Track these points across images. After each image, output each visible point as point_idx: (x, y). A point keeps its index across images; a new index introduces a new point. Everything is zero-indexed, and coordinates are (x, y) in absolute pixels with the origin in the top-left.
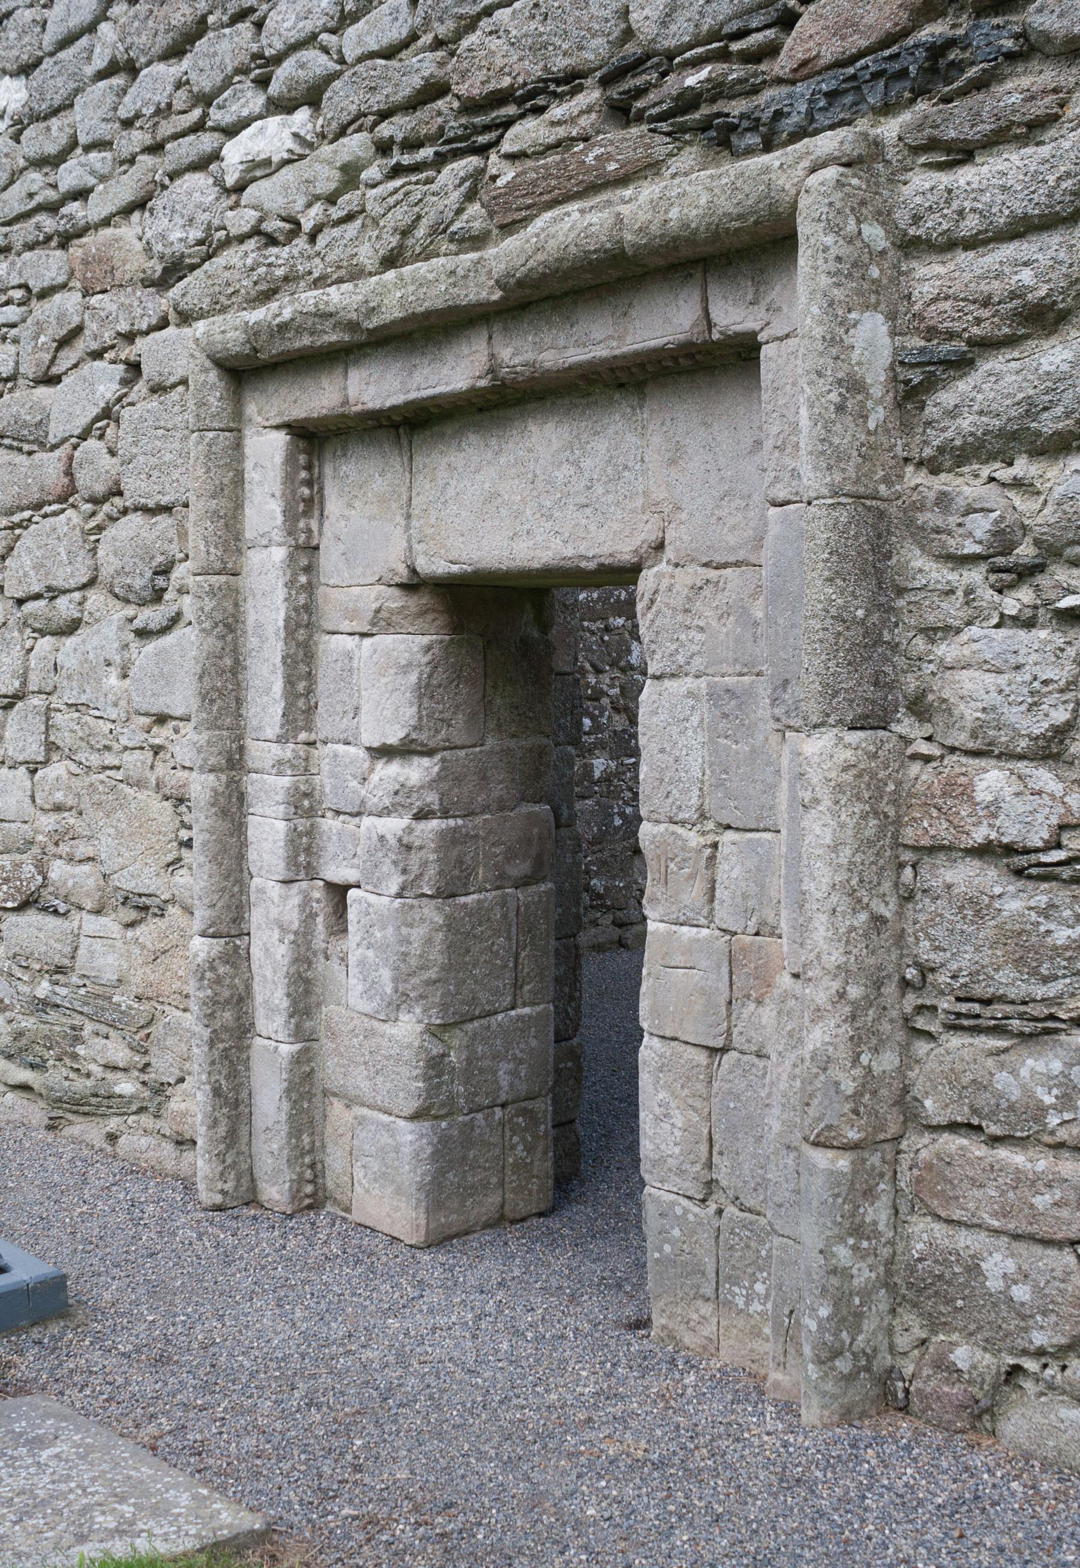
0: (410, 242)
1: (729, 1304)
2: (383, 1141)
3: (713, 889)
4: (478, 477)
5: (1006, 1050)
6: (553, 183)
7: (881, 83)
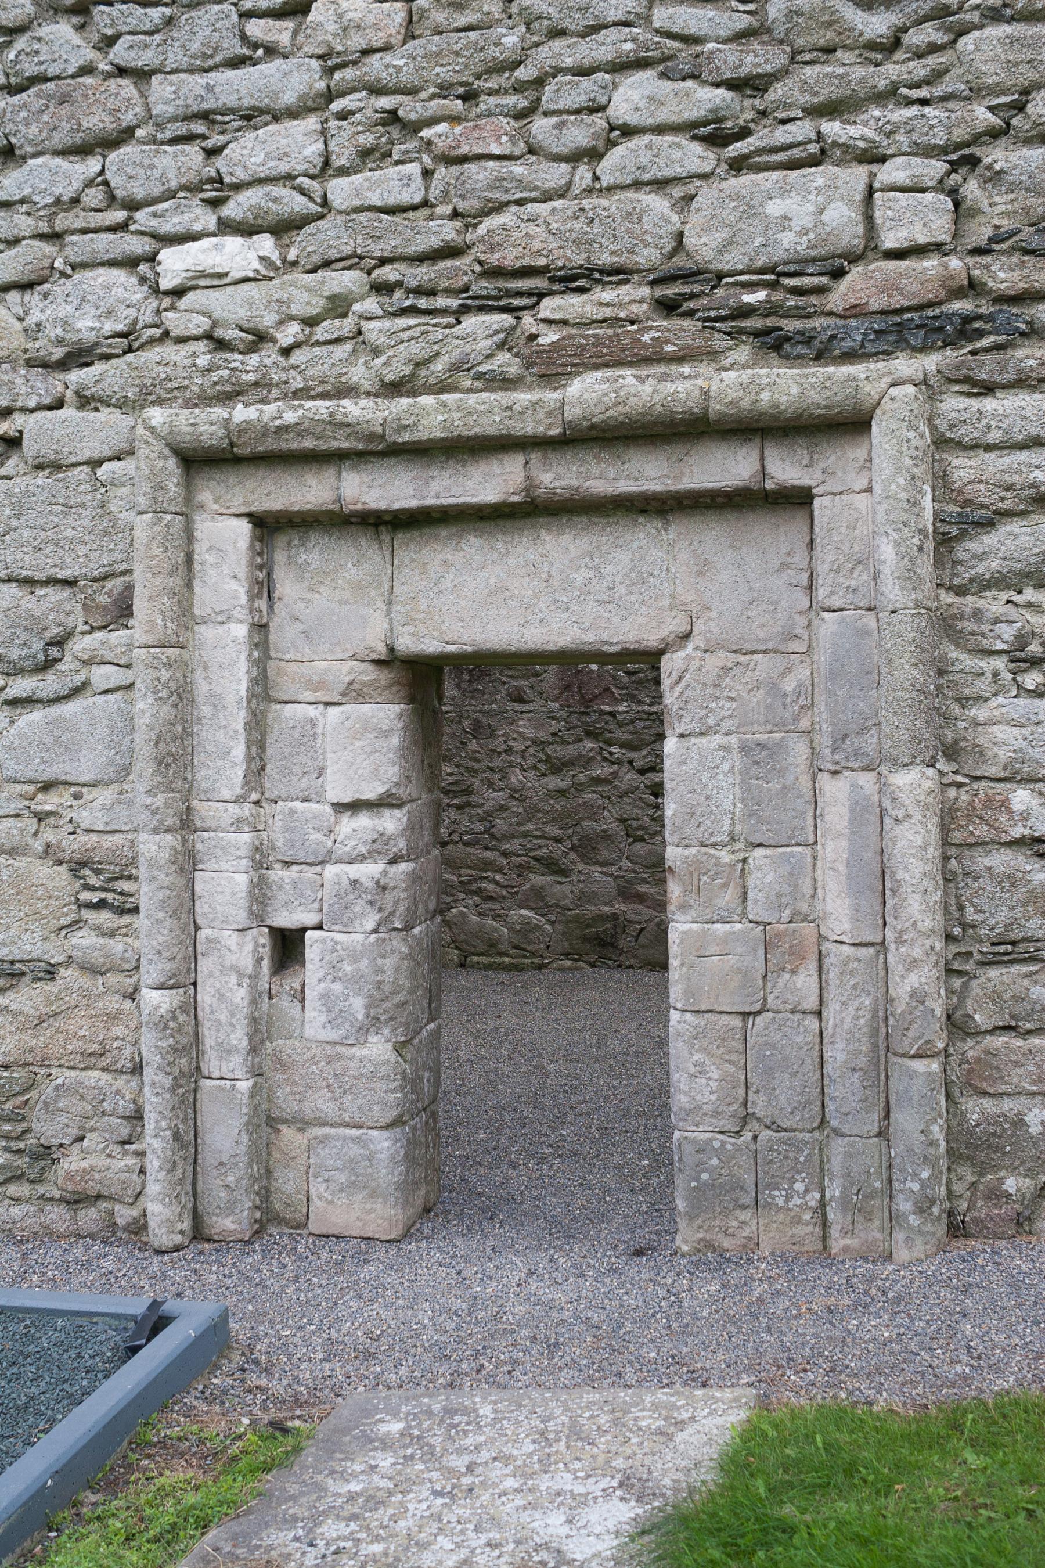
0: (424, 372)
1: (768, 1206)
2: (351, 1153)
3: (746, 893)
4: (481, 574)
5: (1036, 972)
6: (605, 351)
7: (922, 332)
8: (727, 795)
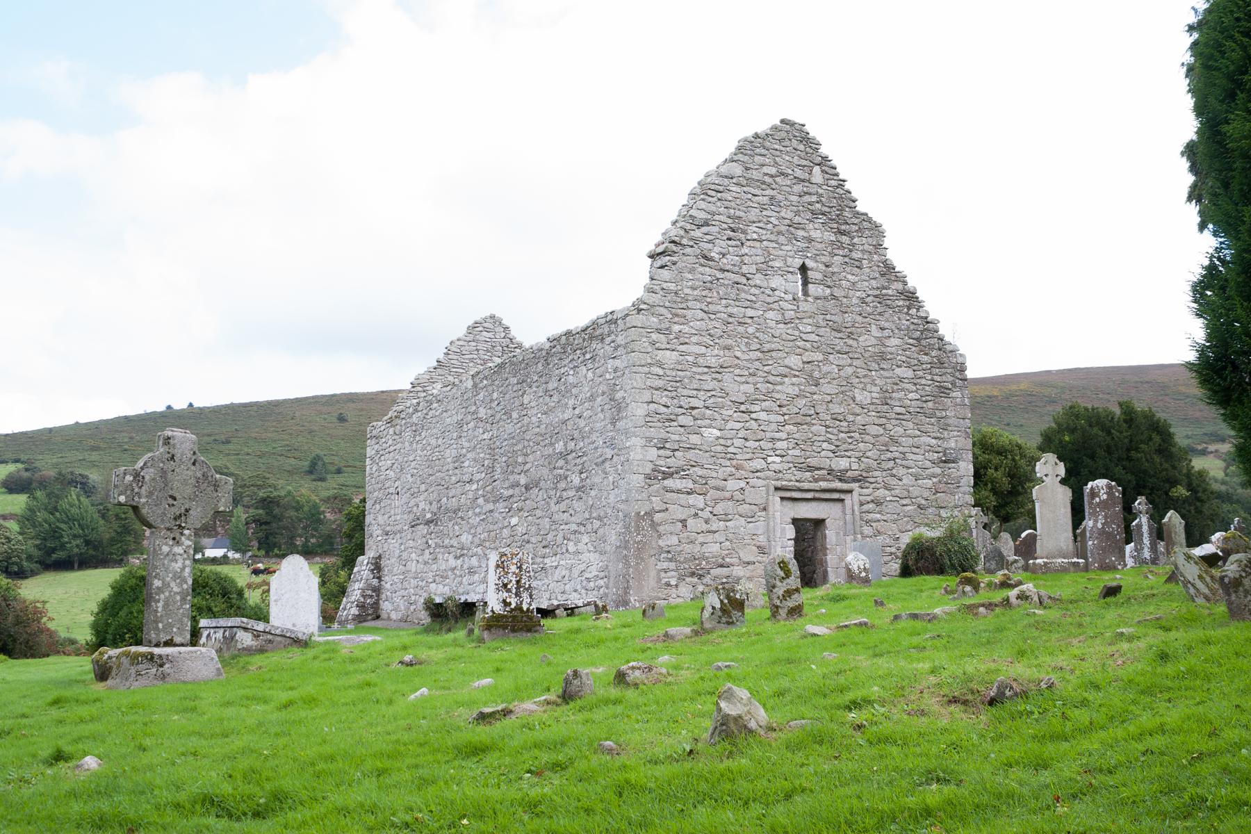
8: (834, 539)
